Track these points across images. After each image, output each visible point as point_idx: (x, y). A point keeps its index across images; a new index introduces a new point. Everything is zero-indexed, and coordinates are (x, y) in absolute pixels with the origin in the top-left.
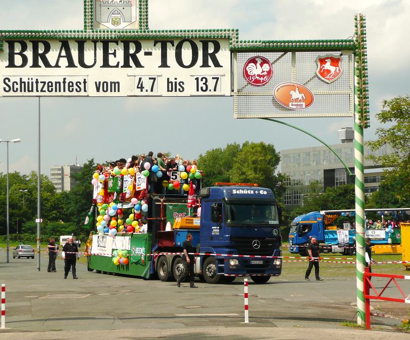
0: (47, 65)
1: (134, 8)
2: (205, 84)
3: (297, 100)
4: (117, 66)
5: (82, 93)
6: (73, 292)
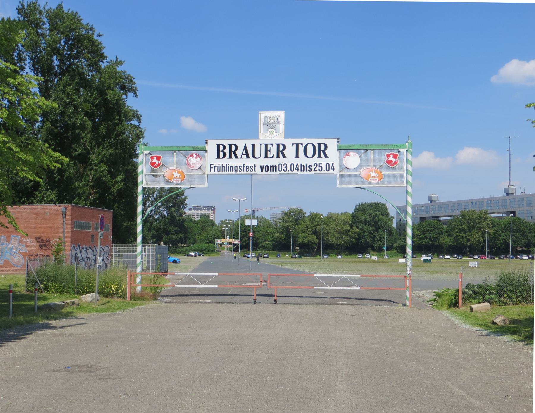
0: (236, 157)
1: (281, 125)
2: (286, 167)
3: (176, 177)
4: (272, 157)
5: (253, 172)
6: (283, 275)
